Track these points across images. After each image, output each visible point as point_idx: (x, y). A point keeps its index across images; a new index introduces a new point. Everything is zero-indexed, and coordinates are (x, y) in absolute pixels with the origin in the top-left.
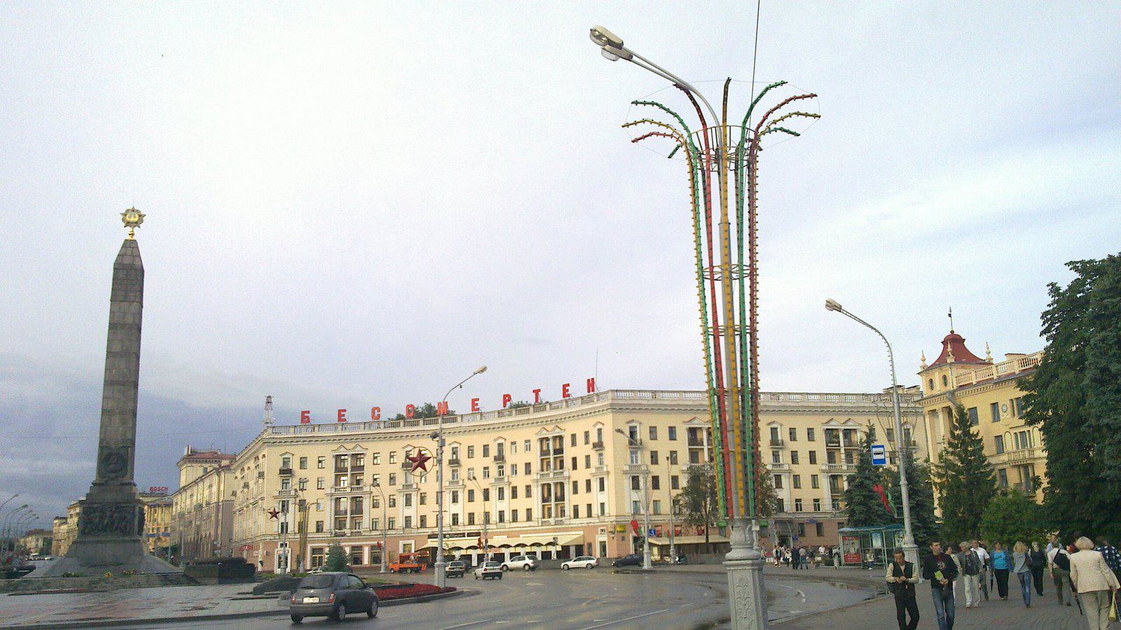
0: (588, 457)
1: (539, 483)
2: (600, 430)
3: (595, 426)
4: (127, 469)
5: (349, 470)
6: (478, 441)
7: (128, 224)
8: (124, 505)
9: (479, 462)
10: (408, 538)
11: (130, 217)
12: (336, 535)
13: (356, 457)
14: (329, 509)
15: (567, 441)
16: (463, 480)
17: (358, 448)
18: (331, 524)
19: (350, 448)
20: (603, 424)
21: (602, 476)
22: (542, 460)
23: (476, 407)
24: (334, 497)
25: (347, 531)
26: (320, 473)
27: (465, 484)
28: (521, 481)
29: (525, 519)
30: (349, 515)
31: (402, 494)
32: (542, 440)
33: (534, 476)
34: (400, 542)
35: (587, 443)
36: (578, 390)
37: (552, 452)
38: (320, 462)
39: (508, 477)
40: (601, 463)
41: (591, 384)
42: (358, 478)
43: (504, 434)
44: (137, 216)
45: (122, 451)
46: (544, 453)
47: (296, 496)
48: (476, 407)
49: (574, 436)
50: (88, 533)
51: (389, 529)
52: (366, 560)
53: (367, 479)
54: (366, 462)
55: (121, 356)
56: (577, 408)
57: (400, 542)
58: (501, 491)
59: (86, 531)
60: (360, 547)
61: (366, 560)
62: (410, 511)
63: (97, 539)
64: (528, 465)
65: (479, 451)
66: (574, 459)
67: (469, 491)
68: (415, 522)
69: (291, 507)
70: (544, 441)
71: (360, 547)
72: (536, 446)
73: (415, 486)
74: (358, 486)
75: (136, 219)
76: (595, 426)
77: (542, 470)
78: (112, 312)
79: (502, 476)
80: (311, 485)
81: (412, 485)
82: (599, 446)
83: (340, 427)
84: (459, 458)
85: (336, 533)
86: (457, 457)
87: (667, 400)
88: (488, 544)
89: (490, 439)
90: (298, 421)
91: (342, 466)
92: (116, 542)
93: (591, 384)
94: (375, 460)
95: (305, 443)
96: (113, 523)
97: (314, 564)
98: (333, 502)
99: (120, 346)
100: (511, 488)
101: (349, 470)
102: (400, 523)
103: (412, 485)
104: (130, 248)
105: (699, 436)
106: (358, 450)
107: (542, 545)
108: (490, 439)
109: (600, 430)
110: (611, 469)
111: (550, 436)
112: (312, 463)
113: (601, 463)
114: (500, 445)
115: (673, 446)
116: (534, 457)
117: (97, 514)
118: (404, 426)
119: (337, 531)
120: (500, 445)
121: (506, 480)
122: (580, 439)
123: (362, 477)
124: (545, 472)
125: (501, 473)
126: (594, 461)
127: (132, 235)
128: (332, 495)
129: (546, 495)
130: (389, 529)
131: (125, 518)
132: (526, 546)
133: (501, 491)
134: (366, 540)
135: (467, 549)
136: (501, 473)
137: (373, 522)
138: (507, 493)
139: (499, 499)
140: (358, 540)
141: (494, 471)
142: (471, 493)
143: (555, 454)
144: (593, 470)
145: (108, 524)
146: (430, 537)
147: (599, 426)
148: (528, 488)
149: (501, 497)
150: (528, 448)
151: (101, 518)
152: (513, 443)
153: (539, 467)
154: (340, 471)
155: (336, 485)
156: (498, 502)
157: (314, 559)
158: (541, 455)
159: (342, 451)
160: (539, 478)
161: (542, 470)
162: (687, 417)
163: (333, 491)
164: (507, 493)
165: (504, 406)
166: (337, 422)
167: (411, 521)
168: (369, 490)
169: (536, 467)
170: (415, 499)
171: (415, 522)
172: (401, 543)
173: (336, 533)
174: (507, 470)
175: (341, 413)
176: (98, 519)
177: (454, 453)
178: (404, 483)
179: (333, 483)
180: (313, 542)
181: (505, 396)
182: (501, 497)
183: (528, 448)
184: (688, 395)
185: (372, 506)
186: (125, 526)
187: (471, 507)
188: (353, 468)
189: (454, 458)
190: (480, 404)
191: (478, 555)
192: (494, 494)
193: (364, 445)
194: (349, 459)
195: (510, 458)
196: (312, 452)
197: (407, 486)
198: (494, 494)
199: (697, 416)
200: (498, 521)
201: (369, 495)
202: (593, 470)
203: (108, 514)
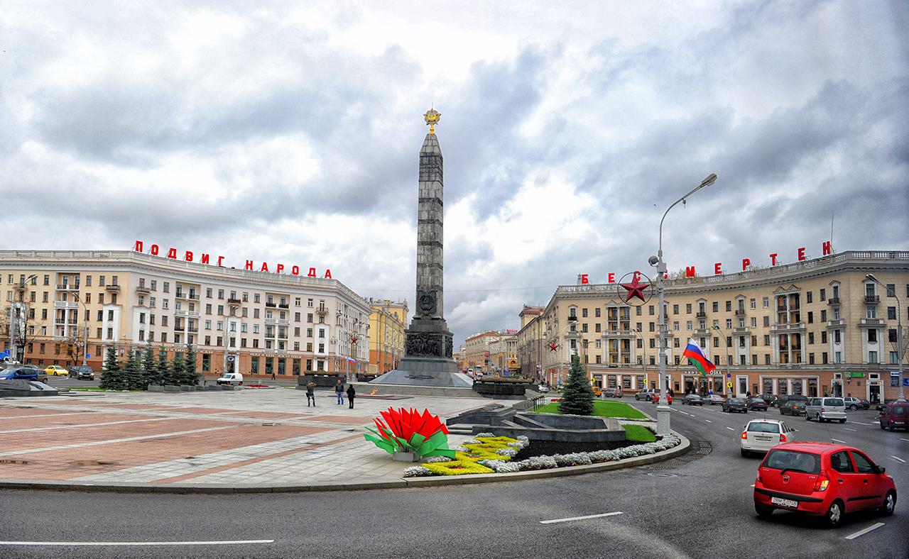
7: (429, 122)
11: (430, 117)
43: (744, 293)
68: (748, 360)
75: (434, 118)
102: (737, 360)
109: (836, 288)
111: (786, 294)
171: (748, 360)
181: (744, 261)
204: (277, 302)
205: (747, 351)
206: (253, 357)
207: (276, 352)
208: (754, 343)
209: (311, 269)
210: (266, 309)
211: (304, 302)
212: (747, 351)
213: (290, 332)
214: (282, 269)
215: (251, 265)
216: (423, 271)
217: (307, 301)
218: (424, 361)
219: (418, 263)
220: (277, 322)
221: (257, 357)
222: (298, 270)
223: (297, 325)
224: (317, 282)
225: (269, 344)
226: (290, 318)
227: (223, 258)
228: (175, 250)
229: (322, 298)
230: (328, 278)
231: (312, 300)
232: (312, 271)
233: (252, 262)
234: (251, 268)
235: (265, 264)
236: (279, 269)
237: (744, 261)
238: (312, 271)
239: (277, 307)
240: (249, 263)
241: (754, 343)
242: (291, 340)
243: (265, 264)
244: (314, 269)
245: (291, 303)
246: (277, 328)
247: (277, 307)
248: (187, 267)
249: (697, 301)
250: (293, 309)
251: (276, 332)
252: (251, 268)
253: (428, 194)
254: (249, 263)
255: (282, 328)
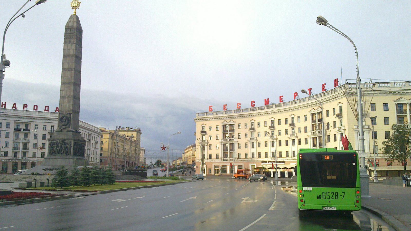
0: (335, 122)
1: (311, 137)
2: (341, 107)
3: (337, 105)
4: (70, 124)
5: (228, 131)
6: (282, 117)
7: (73, 8)
8: (66, 141)
9: (283, 127)
10: (253, 162)
11: (74, 4)
12: (224, 160)
13: (232, 125)
14: (220, 148)
15: (325, 114)
16: (276, 136)
17: (232, 122)
18: (221, 155)
19: (228, 122)
20: (342, 103)
21: (341, 132)
22: (313, 125)
23: (282, 100)
24: (222, 143)
25: (228, 159)
26: (217, 133)
27: (277, 137)
28: (302, 136)
29: (285, 156)
30: (229, 152)
31: (250, 142)
32: (312, 115)
33: (309, 133)
34: (250, 164)
35: (334, 115)
36: (330, 86)
37: (317, 120)
38: (217, 128)
39: (297, 134)
40: (342, 125)
41: (336, 81)
42: (233, 135)
43: (294, 112)
44: (77, 3)
45: (68, 116)
46: (313, 121)
47: (208, 143)
48: (282, 100)
49: (328, 111)
50: (51, 154)
51: (245, 158)
52: (228, 172)
53: (236, 135)
54: (235, 128)
55: (68, 70)
56: (330, 95)
57: (250, 164)
58: (294, 140)
59: (51, 153)
60: (226, 166)
61: (228, 172)
62: (259, 150)
63: (54, 157)
64: (306, 128)
65: (283, 122)
66: (328, 124)
67: (279, 141)
68: (256, 155)
69: (206, 147)
70: (314, 115)
71: (226, 166)
72: (309, 118)
73: (255, 139)
74: (233, 139)
75: (76, 5)
76: (337, 105)
77: (313, 130)
78: (64, 50)
79: (294, 134)
80: (213, 138)
81: (254, 138)
82: (340, 116)
83: (224, 112)
84: (274, 125)
85: (224, 159)
86: (273, 125)
87: (382, 88)
88: (278, 167)
89: (287, 115)
90: (208, 110)
91: (226, 130)
92: (62, 159)
93: (336, 81)
94: (239, 127)
95: (210, 120)
96: (62, 150)
97: (215, 173)
98: (222, 146)
99: (67, 65)
100: (298, 140)
101: (228, 131)
102: (250, 156)
103: (254, 138)
104: (75, 19)
105: (404, 108)
106: (232, 123)
107: (281, 169)
108: (287, 115)
109: (341, 107)
110: (346, 128)
111: (316, 112)
112: (213, 128)
113: (342, 125)
114: (293, 118)
115: (386, 114)
116: (309, 124)
117: (55, 145)
118: (251, 111)
119: (224, 158)
120: (293, 118)
121: (295, 135)
122: (331, 113)
123: (234, 135)
124: (314, 131)
125: (293, 132)
126: (338, 125)
127: (75, 12)
128: (222, 142)
129: (315, 143)
130: (239, 158)
131: (67, 147)
132: (281, 169)
133: (294, 140)
134: (236, 163)
135: (283, 169)
136: (293, 132)
137: (239, 155)
138: (296, 142)
139: (293, 145)
140: (225, 163)
141: (290, 131)
142: (280, 142)
143: (319, 122)
144: (337, 129)
145: (59, 150)
146: (262, 162)
147: (340, 105)
148: (306, 139)
149: (294, 144)
150: (306, 119)
151: (57, 147)
152: (299, 117)
153: (311, 129)
154: (225, 131)
155: (223, 138)
156: (292, 146)
157: (215, 170)
158: (312, 122)
159: (225, 123)
160: (311, 134)
161: (313, 130)
162: (397, 97)
163: (222, 140)
164: (296, 142)
165: (295, 99)
166: (223, 110)
167: (254, 155)
168: (236, 141)
169: (309, 128)
170: (256, 145)
171: (256, 155)
172: (250, 165)
173: (224, 159)
174: (296, 130)
175: (225, 106)
176: (55, 148)
177: (272, 123)
178: (251, 137)
179: (222, 137)
180: (215, 163)
181: (295, 94)
182: (294, 144)
183: (306, 119)
184: (396, 84)
185: (238, 148)
186: (67, 151)
187: (266, 150)
188: (230, 131)
189: (272, 125)
190: (284, 99)
191: (281, 172)
192: (290, 142)
193: (234, 120)
194: (228, 127)
195: (297, 125)
196: (213, 123)
197: (252, 139)
198: (290, 142)
199: (402, 96)
200: (292, 156)
201: (236, 143)
202: (337, 129)
203: (60, 145)
204: (22, 127)
205: (256, 150)
206: (3, 162)
207: (20, 158)
208: (259, 146)
209: (46, 107)
210: (14, 132)
211: (41, 127)
212: (256, 150)
213: (30, 146)
214: (27, 107)
215: (5, 105)
216: (63, 101)
217: (43, 127)
218: (59, 158)
219: (61, 96)
220: (22, 140)
221: (6, 162)
222: (48, 109)
223: (35, 141)
224: (37, 113)
225: (15, 154)
226: (31, 137)
227: (282, 96)
228: (48, 107)
229: (45, 124)
230: (14, 108)
231: (37, 125)
232: (47, 108)
233: (5, 103)
234: (5, 107)
235: (15, 104)
236: (24, 107)
237: (295, 94)
238: (47, 108)
239: (22, 130)
240: (4, 103)
241: (259, 146)
242: (31, 150)
243: (15, 104)
244: (48, 107)
245: (32, 127)
246: (21, 144)
247: (22, 130)
248: (12, 112)
249: (270, 119)
250: (33, 131)
251: (21, 146)
252: (5, 107)
253: (69, 52)
254: (4, 103)
255: (25, 145)
